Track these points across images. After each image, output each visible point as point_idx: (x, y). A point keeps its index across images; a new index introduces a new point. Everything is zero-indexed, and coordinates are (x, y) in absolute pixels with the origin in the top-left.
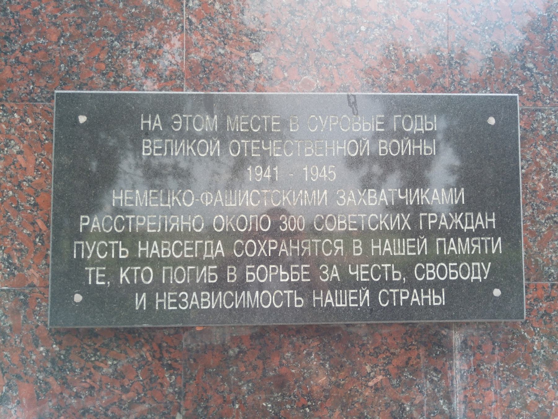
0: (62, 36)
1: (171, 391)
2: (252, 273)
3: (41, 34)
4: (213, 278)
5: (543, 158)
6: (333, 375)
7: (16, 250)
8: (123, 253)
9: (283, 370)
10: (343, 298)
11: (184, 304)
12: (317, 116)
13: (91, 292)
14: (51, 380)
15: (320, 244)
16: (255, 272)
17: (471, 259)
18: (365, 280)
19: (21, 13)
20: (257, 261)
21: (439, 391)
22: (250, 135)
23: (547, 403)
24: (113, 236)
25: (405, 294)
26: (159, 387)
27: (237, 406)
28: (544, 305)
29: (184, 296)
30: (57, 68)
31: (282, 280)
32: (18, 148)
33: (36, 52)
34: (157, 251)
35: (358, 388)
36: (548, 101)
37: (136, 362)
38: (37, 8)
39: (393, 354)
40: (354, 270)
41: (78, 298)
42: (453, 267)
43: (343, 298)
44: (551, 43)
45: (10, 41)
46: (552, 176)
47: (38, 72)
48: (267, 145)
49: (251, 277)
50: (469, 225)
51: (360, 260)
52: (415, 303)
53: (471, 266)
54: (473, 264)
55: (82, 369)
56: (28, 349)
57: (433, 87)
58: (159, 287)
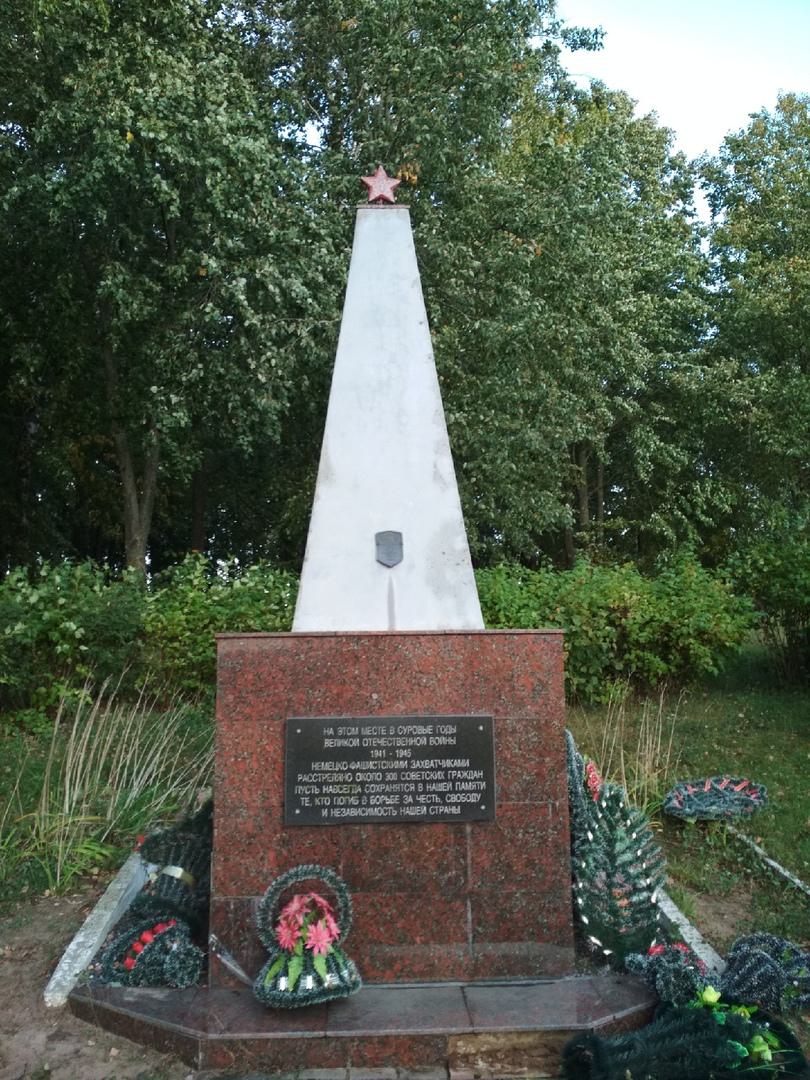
8: (316, 791)
13: (303, 808)
24: (313, 783)
47: (275, 706)
51: (422, 793)
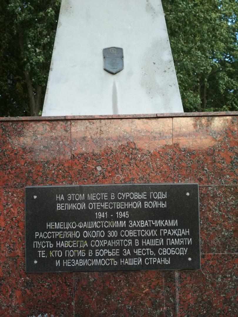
0: (26, 163)
1: (69, 294)
2: (98, 253)
3: (17, 162)
4: (84, 254)
5: (211, 205)
6: (130, 288)
7: (12, 243)
8: (51, 246)
9: (111, 287)
10: (132, 261)
11: (73, 264)
12: (121, 193)
13: (40, 260)
14: (26, 289)
15: (123, 242)
16: (99, 252)
17: (179, 246)
18: (140, 255)
19: (11, 155)
20: (100, 248)
21: (170, 295)
22: (97, 201)
23: (211, 298)
24: (47, 239)
25: (155, 260)
26: (65, 293)
27: (94, 300)
28: (211, 262)
29: (73, 261)
30: (24, 175)
31: (109, 255)
32: (11, 205)
33: (16, 169)
34: (63, 245)
35: (139, 293)
36: (213, 183)
37: (56, 284)
38: (16, 152)
39: (152, 281)
40: (136, 251)
41: (36, 262)
42: (173, 250)
43: (132, 261)
44: (214, 160)
45: (7, 165)
46: (215, 212)
48: (103, 205)
49: (97, 254)
50: (179, 234)
51: (138, 247)
52: (159, 263)
53: (180, 249)
54: (181, 248)
55: (37, 286)
56: (18, 279)
57: (167, 178)
58: (64, 258)
